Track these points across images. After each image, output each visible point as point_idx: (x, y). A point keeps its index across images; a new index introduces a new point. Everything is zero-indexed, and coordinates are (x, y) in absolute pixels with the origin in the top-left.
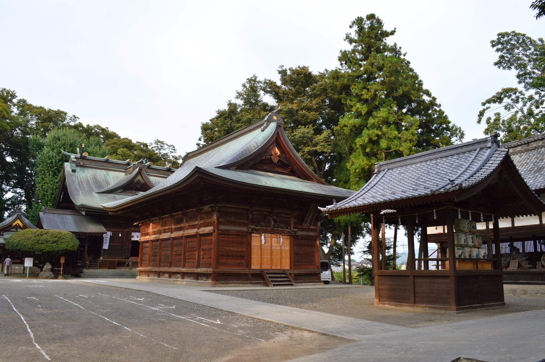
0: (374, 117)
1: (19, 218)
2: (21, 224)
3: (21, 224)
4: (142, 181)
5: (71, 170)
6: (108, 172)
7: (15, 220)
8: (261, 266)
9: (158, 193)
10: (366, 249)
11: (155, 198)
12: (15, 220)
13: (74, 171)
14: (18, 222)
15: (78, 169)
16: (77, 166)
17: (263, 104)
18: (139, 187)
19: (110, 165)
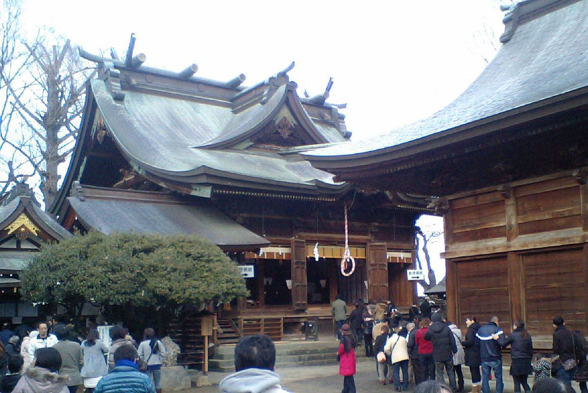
0: (61, 159)
1: (25, 211)
2: (32, 228)
3: (32, 228)
4: (292, 121)
5: (109, 96)
6: (195, 104)
7: (13, 217)
8: (470, 378)
9: (507, 119)
10: (111, 343)
11: (462, 145)
12: (13, 217)
13: (119, 98)
14: (23, 221)
15: (128, 95)
16: (123, 88)
17: (192, 67)
18: (286, 134)
19: (193, 88)
